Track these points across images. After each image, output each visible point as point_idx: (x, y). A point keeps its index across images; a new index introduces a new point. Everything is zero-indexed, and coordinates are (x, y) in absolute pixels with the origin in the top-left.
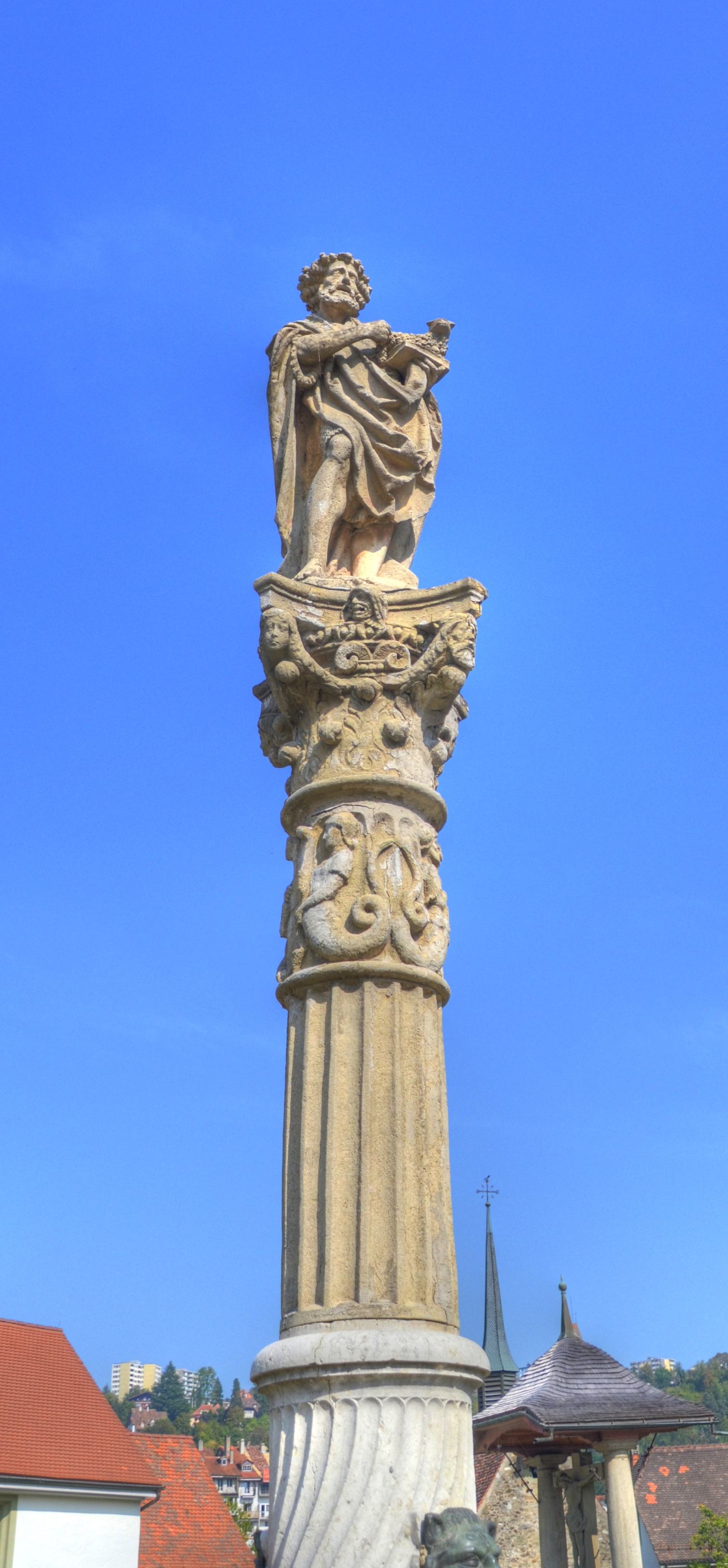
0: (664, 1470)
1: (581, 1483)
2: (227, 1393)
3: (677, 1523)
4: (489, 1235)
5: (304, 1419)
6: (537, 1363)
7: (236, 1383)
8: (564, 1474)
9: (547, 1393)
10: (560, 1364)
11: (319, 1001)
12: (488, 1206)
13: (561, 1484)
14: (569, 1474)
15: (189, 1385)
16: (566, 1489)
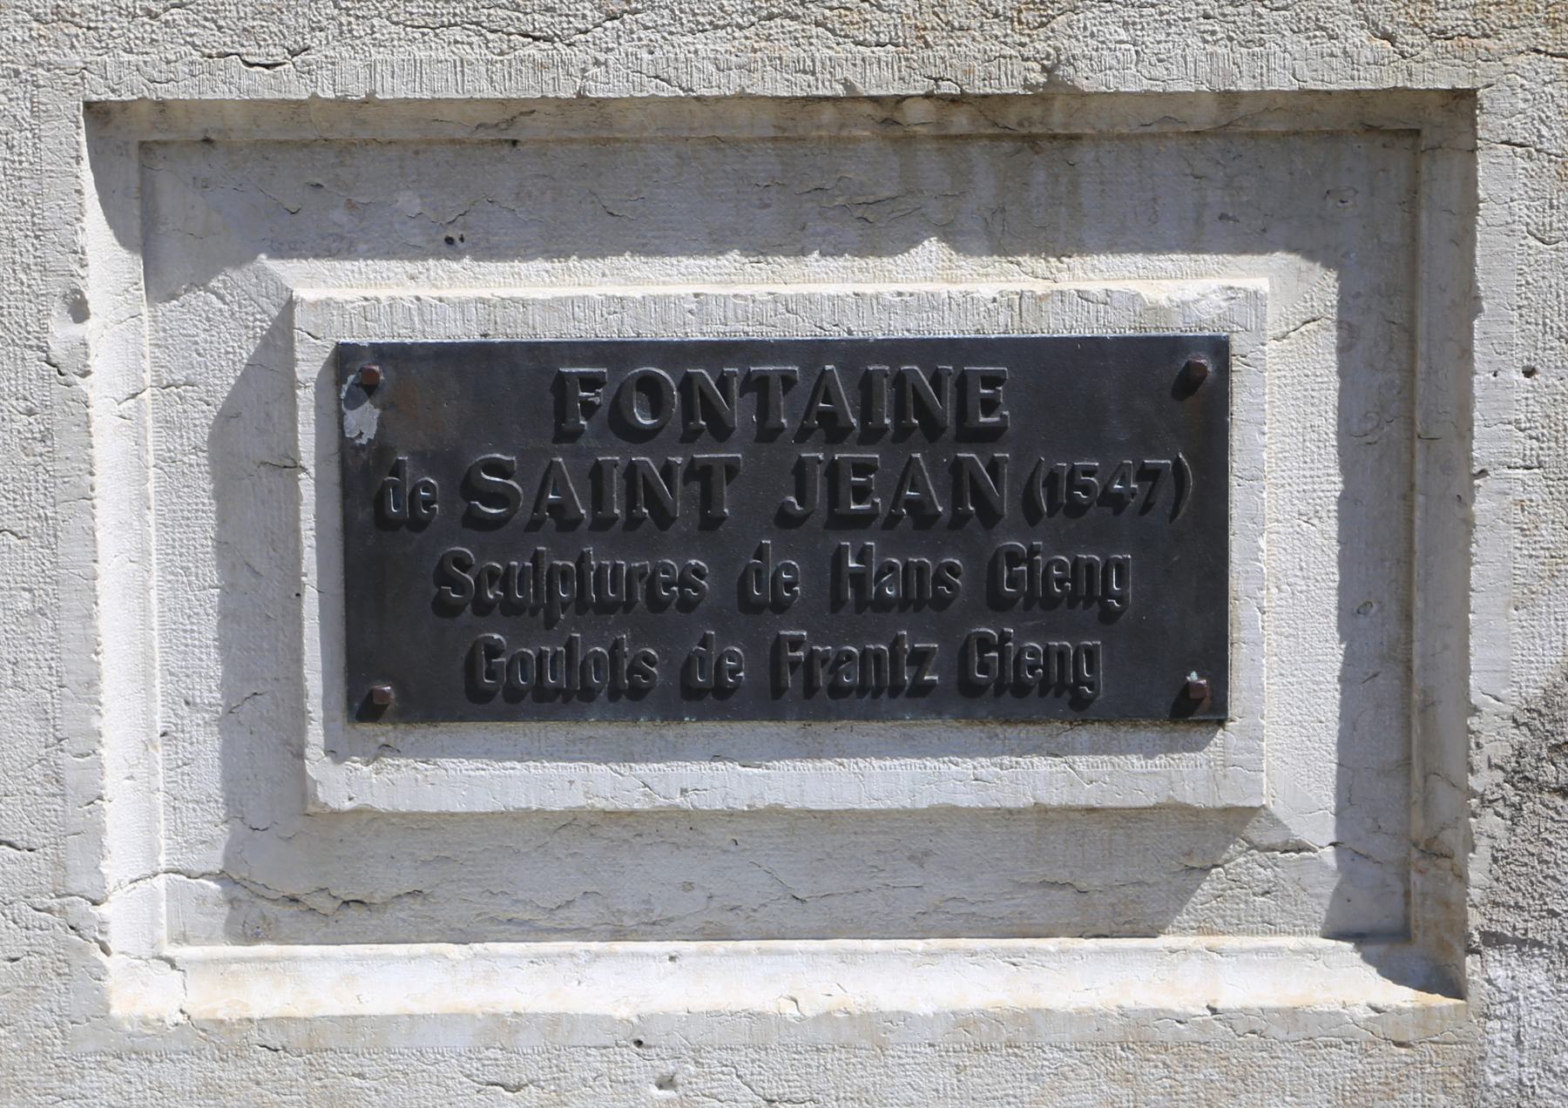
5: (932, 248)
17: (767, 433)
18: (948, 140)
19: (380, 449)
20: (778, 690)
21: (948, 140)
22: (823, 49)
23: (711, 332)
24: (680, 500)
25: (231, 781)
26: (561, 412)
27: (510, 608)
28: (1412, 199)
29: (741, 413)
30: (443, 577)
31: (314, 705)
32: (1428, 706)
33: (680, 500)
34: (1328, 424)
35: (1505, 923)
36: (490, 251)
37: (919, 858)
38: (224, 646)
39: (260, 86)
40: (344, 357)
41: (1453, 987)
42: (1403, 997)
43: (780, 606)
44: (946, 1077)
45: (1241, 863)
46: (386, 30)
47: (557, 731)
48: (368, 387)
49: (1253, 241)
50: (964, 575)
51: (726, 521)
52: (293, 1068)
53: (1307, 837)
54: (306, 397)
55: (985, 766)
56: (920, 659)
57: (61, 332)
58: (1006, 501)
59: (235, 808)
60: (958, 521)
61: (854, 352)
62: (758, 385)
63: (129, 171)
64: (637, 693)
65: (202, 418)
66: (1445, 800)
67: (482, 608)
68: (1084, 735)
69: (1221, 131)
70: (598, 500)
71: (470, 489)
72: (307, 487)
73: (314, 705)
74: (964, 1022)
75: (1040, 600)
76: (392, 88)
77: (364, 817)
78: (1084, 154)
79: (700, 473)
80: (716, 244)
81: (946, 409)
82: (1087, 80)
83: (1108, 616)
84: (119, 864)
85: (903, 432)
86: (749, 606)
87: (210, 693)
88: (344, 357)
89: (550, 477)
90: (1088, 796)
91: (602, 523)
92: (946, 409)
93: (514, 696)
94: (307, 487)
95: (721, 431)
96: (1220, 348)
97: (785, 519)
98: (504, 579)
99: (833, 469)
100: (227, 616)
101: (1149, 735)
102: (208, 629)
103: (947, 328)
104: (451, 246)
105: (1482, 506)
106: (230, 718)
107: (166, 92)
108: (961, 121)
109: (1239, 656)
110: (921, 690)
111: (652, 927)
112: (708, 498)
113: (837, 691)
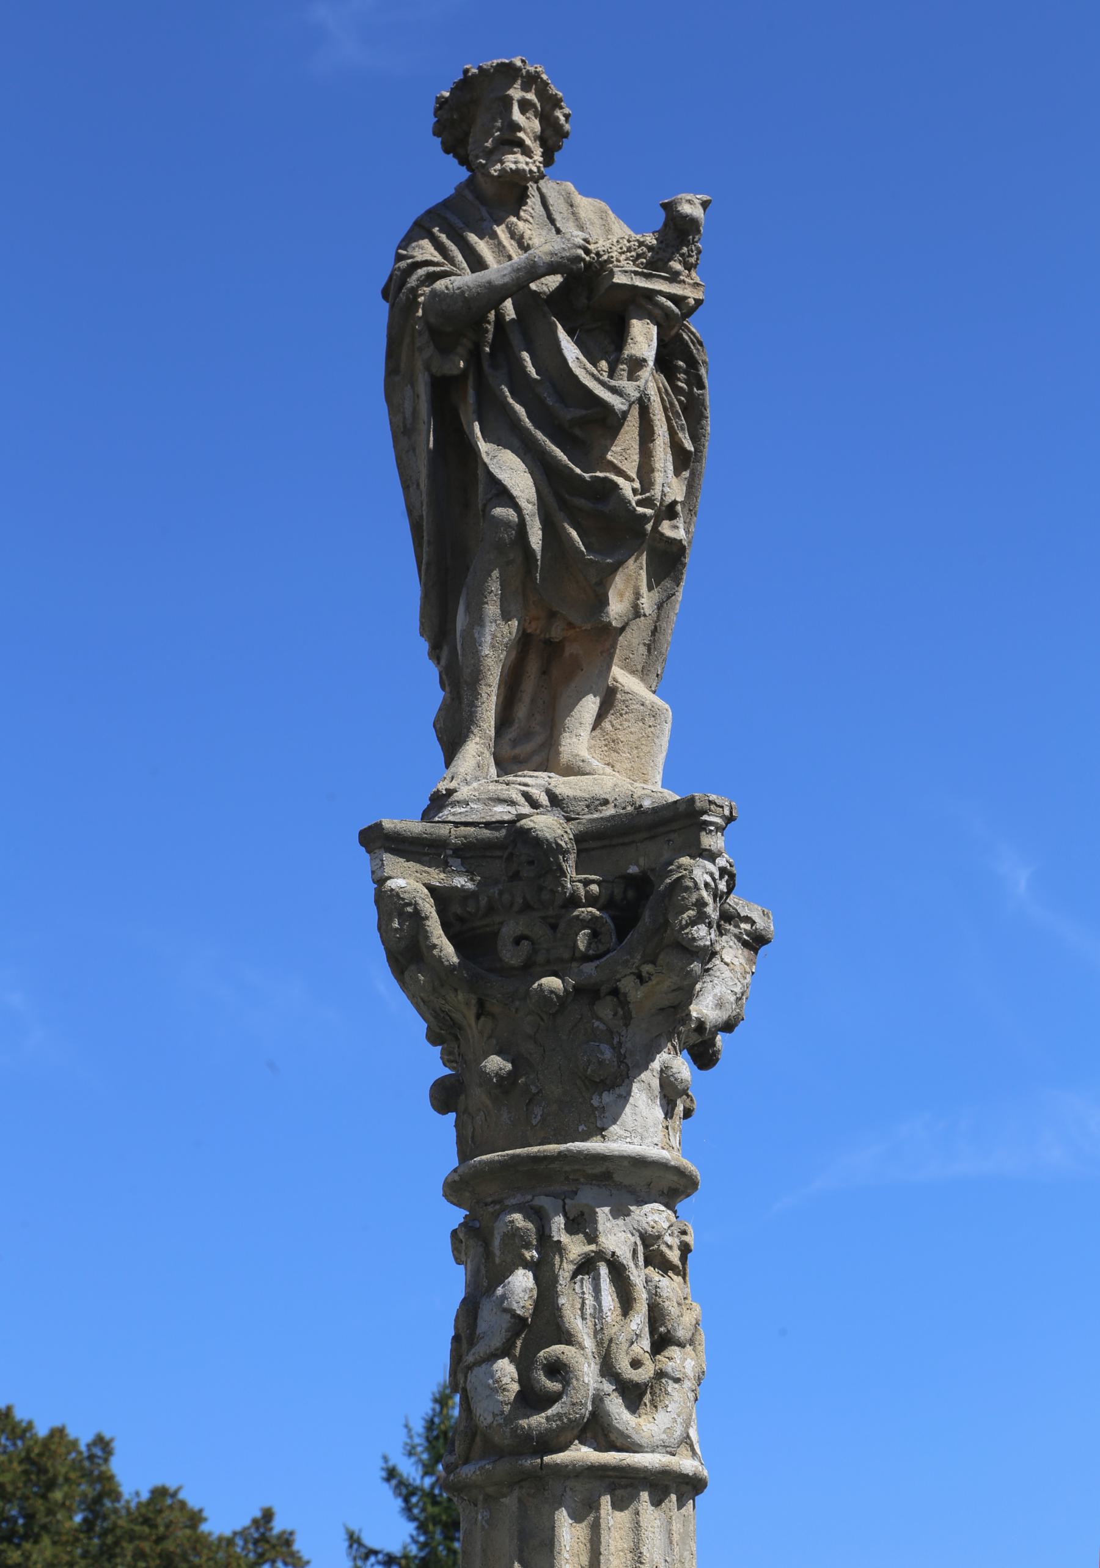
11: (577, 1517)
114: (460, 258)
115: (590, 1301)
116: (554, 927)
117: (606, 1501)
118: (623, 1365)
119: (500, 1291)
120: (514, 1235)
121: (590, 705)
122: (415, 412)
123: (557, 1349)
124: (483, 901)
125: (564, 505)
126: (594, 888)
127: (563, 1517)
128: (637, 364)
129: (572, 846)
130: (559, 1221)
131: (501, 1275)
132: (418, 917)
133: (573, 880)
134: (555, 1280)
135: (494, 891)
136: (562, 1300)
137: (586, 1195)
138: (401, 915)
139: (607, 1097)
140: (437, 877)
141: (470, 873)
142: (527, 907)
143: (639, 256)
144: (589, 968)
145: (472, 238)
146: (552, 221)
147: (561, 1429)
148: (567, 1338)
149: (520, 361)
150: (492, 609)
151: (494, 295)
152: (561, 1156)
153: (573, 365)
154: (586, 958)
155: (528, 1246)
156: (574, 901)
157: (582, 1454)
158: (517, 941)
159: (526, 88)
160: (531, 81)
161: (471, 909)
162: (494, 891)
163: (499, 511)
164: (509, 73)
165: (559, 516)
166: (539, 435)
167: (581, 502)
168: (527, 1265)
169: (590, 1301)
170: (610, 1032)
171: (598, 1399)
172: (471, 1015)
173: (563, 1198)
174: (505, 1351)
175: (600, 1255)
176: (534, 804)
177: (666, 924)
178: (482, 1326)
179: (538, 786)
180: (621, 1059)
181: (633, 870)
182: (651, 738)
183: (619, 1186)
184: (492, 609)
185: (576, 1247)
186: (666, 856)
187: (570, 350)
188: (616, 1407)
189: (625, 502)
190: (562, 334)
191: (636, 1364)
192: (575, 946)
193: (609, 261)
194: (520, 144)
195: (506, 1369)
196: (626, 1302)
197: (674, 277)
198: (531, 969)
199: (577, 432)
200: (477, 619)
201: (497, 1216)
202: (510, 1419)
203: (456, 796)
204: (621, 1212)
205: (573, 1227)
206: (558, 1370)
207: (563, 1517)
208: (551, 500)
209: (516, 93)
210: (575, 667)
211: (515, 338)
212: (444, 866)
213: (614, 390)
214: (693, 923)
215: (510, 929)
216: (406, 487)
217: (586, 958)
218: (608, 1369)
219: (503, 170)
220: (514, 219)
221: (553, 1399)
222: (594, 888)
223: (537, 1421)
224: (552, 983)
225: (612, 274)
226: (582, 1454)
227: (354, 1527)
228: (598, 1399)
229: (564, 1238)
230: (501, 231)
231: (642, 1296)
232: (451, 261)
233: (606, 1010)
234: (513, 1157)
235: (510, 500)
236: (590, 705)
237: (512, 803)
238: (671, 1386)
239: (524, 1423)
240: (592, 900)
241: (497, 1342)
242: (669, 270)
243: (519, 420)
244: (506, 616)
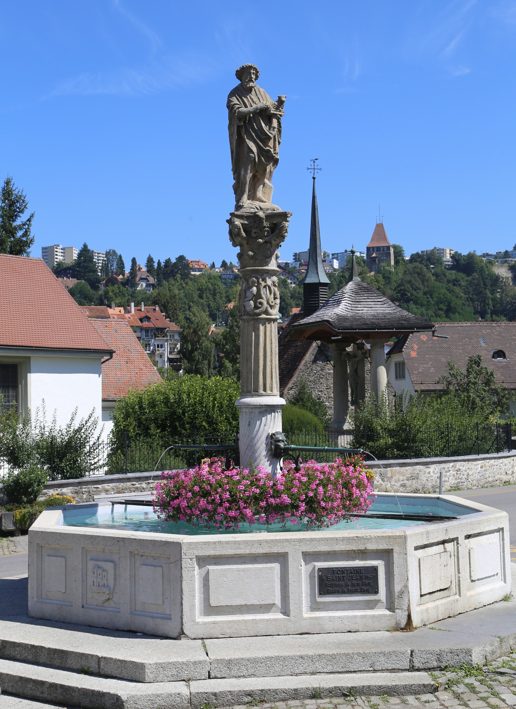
0: (424, 337)
1: (357, 359)
2: (127, 270)
3: (429, 368)
4: (314, 198)
5: (357, 560)
6: (336, 294)
7: (134, 261)
8: (348, 353)
9: (341, 313)
10: (348, 296)
11: (263, 325)
12: (314, 178)
13: (346, 359)
14: (351, 354)
15: (99, 260)
16: (349, 361)
17: (347, 573)
18: (358, 553)
19: (321, 575)
20: (348, 592)
21: (358, 553)
22: (351, 547)
23: (343, 566)
24: (341, 578)
25: (310, 600)
26: (333, 572)
27: (330, 586)
28: (389, 556)
29: (346, 572)
30: (326, 584)
31: (317, 594)
32: (392, 592)
33: (341, 578)
34: (384, 572)
35: (398, 607)
36: (328, 561)
37: (358, 604)
38: (310, 590)
39: (313, 550)
40: (319, 569)
41: (395, 612)
42: (391, 613)
43: (348, 586)
44: (360, 620)
45: (379, 604)
46: (322, 546)
47: (333, 595)
48: (320, 571)
49: (379, 559)
50: (431, 268)
51: (29, 581)
52: (316, 620)
53: (383, 602)
54: (316, 572)
55: (362, 597)
56: (358, 589)
57: (300, 568)
58: (363, 578)
59: (311, 602)
60: (360, 579)
61: (353, 567)
62: (347, 570)
63: (304, 556)
64: (339, 592)
65: (309, 573)
66: (393, 599)
67: (328, 586)
68: (369, 595)
69: (376, 552)
70: (336, 578)
71: (327, 578)
72: (316, 578)
73: (317, 594)
74: (362, 616)
75: (366, 585)
76: (322, 550)
77: (320, 602)
78: (367, 554)
79: (343, 576)
80: (343, 561)
81: (359, 572)
82: (368, 548)
83: (371, 586)
84: (304, 606)
85: (356, 573)
86: (346, 586)
87: (309, 594)
88: (319, 569)
89: (333, 577)
90: (369, 599)
91: (336, 580)
92: (359, 572)
93: (330, 593)
94: (316, 578)
95: (344, 573)
96: (377, 567)
97: (349, 580)
98: (330, 584)
99: (352, 576)
100: (310, 588)
101: (373, 595)
102: (309, 589)
103: (359, 566)
104: (325, 561)
105: (395, 577)
106: (310, 595)
107: (307, 551)
108: (359, 552)
109: (379, 588)
110: (358, 592)
111: (339, 610)
112: (343, 578)
113: (352, 592)
114: (241, 102)
115: (265, 292)
116: (261, 231)
117: (267, 323)
118: (271, 303)
119: (251, 290)
120: (253, 281)
121: (262, 186)
122: (234, 131)
123: (260, 300)
124: (249, 226)
125: (261, 153)
126: (268, 225)
127: (261, 325)
128: (274, 128)
129: (264, 218)
130: (261, 279)
131: (251, 287)
132: (240, 229)
133: (265, 224)
134: (260, 289)
135: (252, 224)
136: (261, 292)
137: (265, 275)
138: (237, 228)
139: (269, 259)
140: (242, 221)
141: (247, 221)
142: (257, 227)
143: (274, 107)
144: (267, 238)
145: (243, 98)
146: (257, 95)
147: (261, 312)
148: (262, 298)
149: (254, 125)
150: (249, 172)
151: (250, 112)
152: (262, 269)
153: (264, 128)
154: (266, 236)
155: (256, 283)
156: (265, 227)
157: (263, 316)
158: (255, 233)
159: (254, 70)
160: (255, 69)
161: (247, 227)
162: (252, 224)
163: (251, 155)
164: (251, 67)
165: (261, 155)
166: (258, 140)
167: (264, 153)
168: (255, 286)
169: (265, 292)
170: (269, 248)
171: (267, 308)
172: (246, 244)
173: (261, 275)
174: (252, 300)
175: (267, 285)
176: (258, 209)
177: (281, 232)
178: (247, 295)
179: (258, 205)
180: (271, 253)
181: (275, 222)
182: (270, 192)
183: (270, 274)
184: (249, 172)
185: (263, 284)
186: (280, 221)
187: (263, 125)
188: (269, 309)
189: (272, 154)
190: (262, 121)
191: (272, 302)
192: (264, 234)
193: (269, 107)
194: (252, 81)
195: (252, 302)
196: (270, 293)
197: (280, 111)
198: (257, 238)
199: (264, 140)
200: (246, 173)
201: (250, 278)
202: (253, 310)
203: (244, 206)
204: (270, 278)
205: (263, 280)
206: (261, 303)
207: (261, 325)
208: (259, 152)
209: (252, 71)
210: (259, 180)
211: (253, 121)
212: (243, 219)
213: (271, 133)
214: (285, 233)
215: (254, 231)
216: (231, 144)
217: (266, 236)
218: (268, 303)
219: (249, 86)
220: (250, 95)
221: (260, 308)
222: (268, 225)
223: (258, 311)
224: (261, 240)
225: (270, 111)
226: (263, 316)
227: (152, 256)
228: (267, 308)
229: (261, 282)
230: (248, 96)
231: (273, 291)
232: (240, 102)
233: (269, 245)
234: (254, 269)
235: (253, 153)
236: (262, 186)
237: (254, 209)
238: (277, 305)
239: (255, 311)
240: (268, 227)
241: (251, 298)
242: (279, 110)
243: (254, 137)
244: (251, 173)
